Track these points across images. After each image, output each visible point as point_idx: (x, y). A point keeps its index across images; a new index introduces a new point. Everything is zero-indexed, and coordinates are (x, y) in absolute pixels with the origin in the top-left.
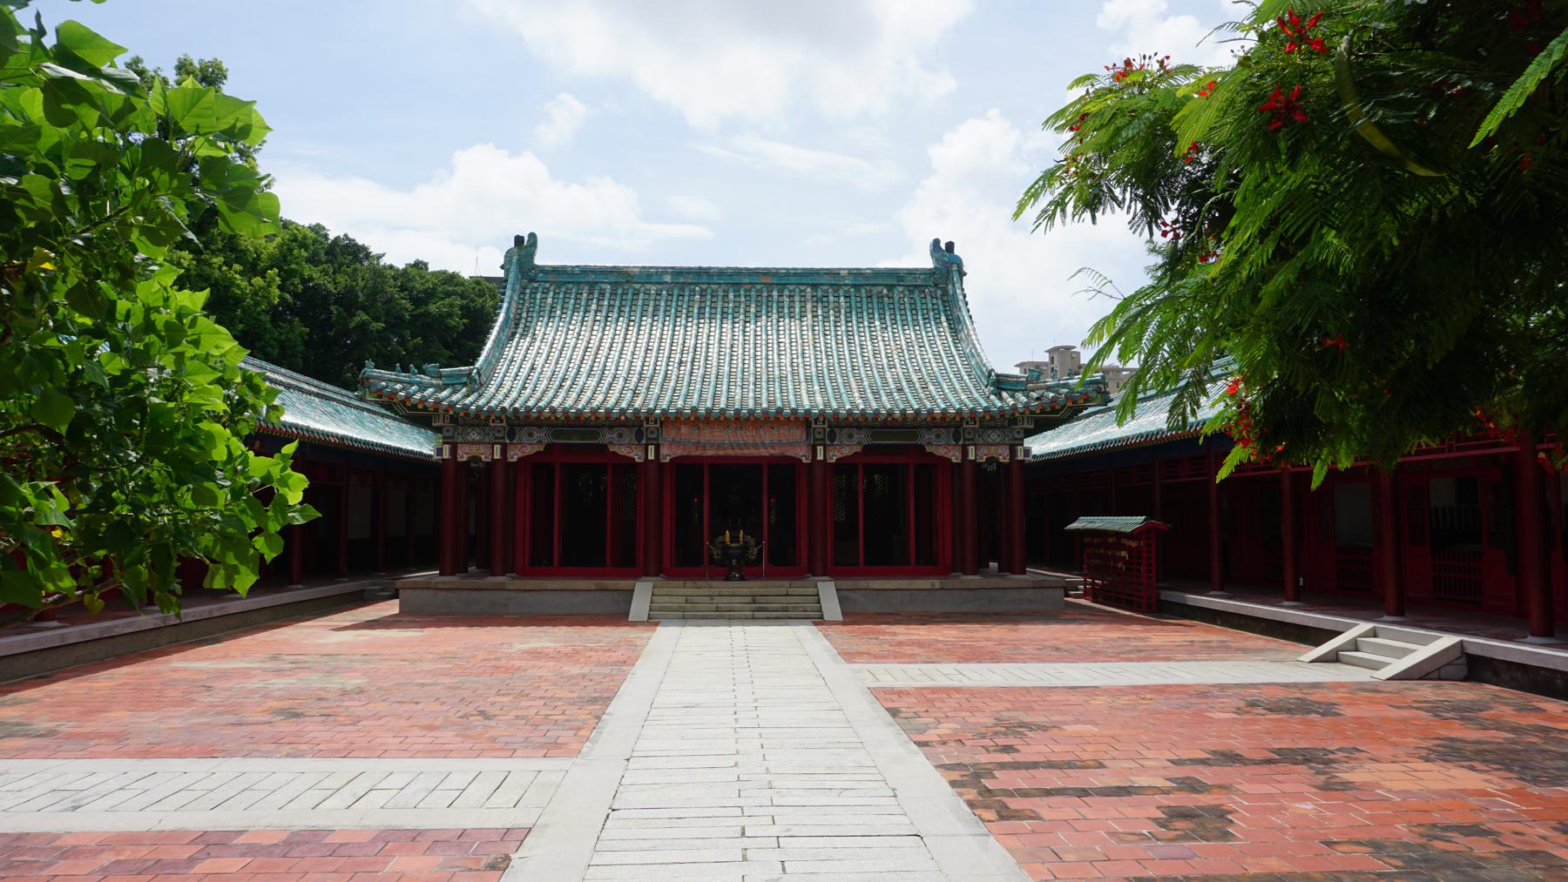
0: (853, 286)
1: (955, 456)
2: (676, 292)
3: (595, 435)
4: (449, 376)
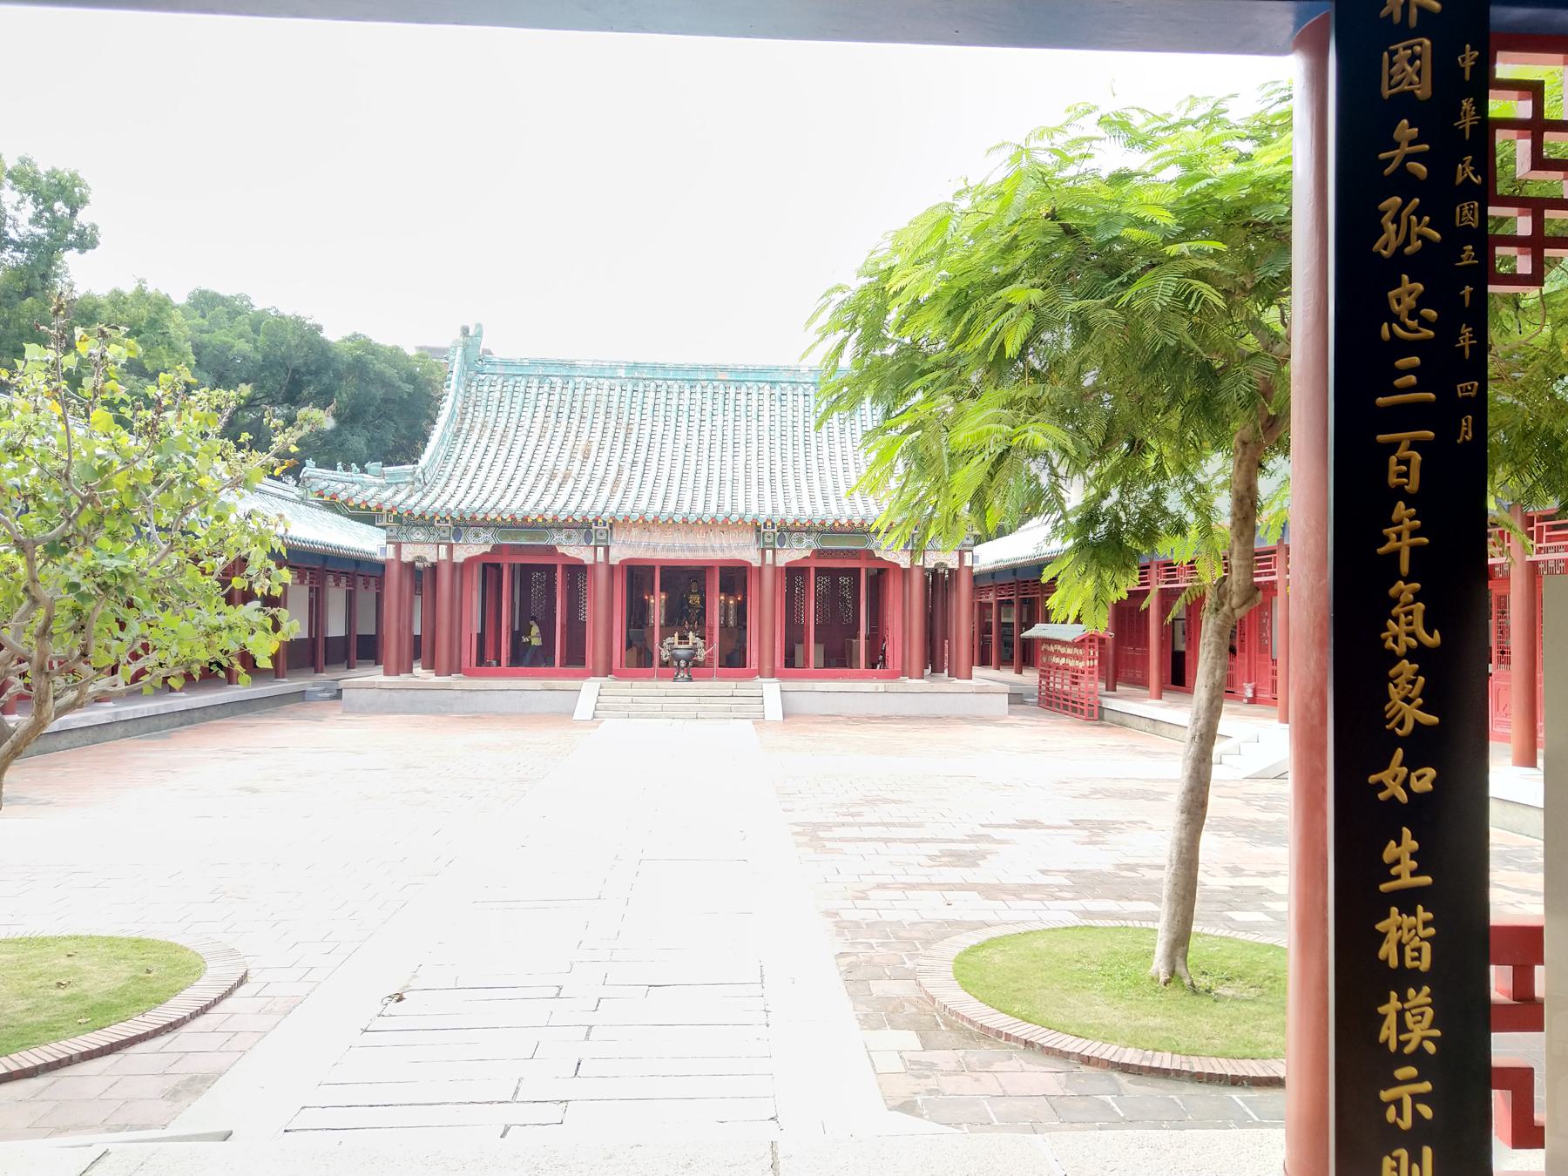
2: (630, 388)
4: (392, 475)
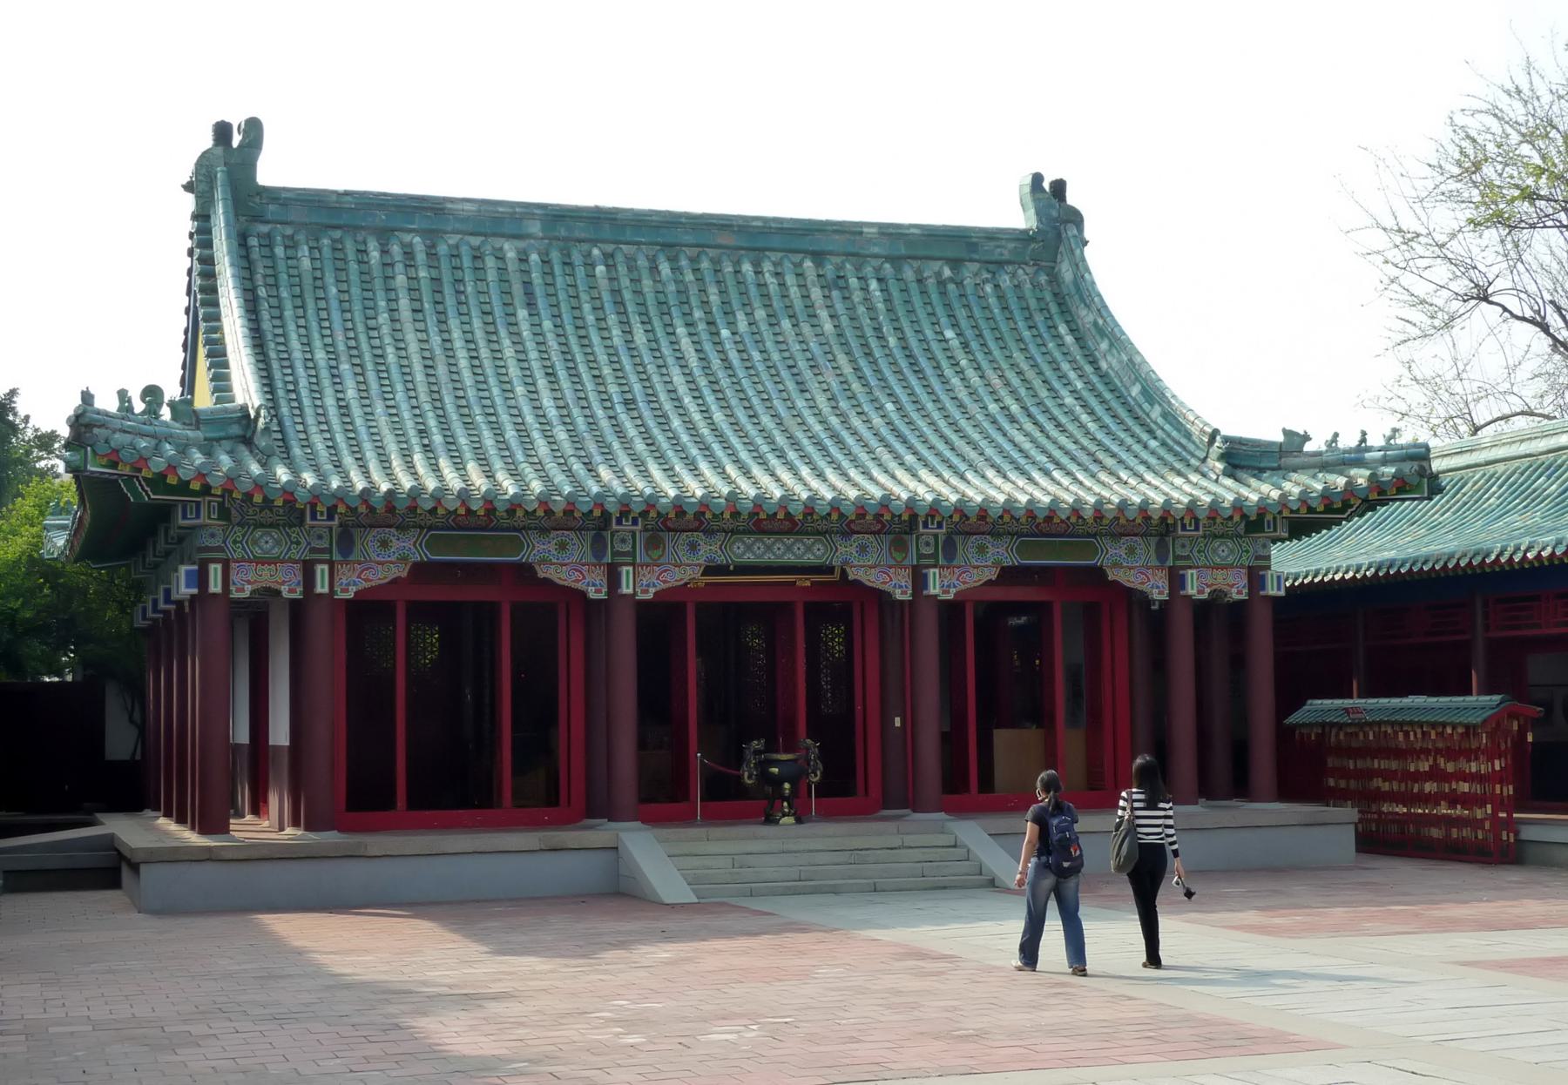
0: (889, 259)
1: (1157, 589)
3: (518, 546)
